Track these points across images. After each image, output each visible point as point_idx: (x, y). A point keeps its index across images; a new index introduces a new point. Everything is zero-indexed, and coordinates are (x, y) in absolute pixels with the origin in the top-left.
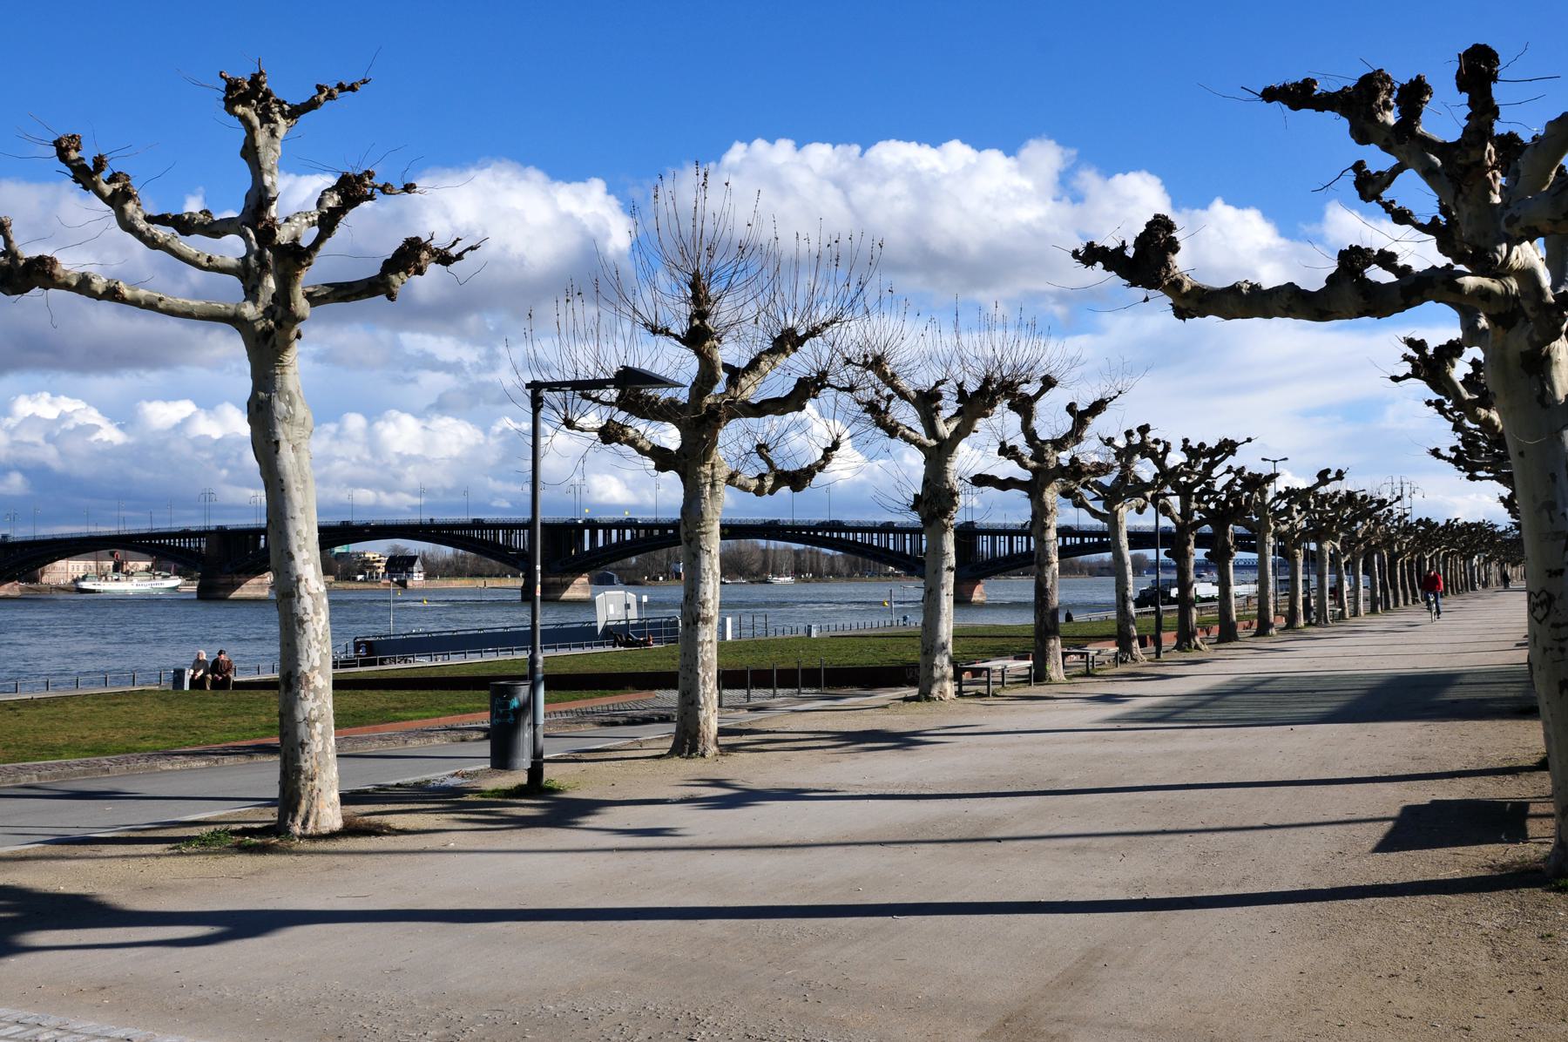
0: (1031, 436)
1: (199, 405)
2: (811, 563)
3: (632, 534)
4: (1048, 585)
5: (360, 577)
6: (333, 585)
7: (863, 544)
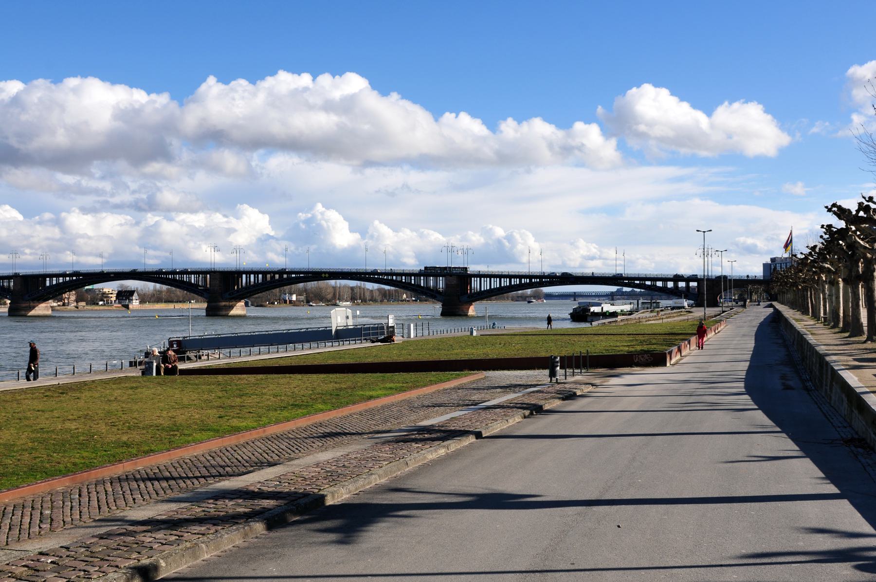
2: (360, 294)
5: (101, 303)
6: (85, 308)
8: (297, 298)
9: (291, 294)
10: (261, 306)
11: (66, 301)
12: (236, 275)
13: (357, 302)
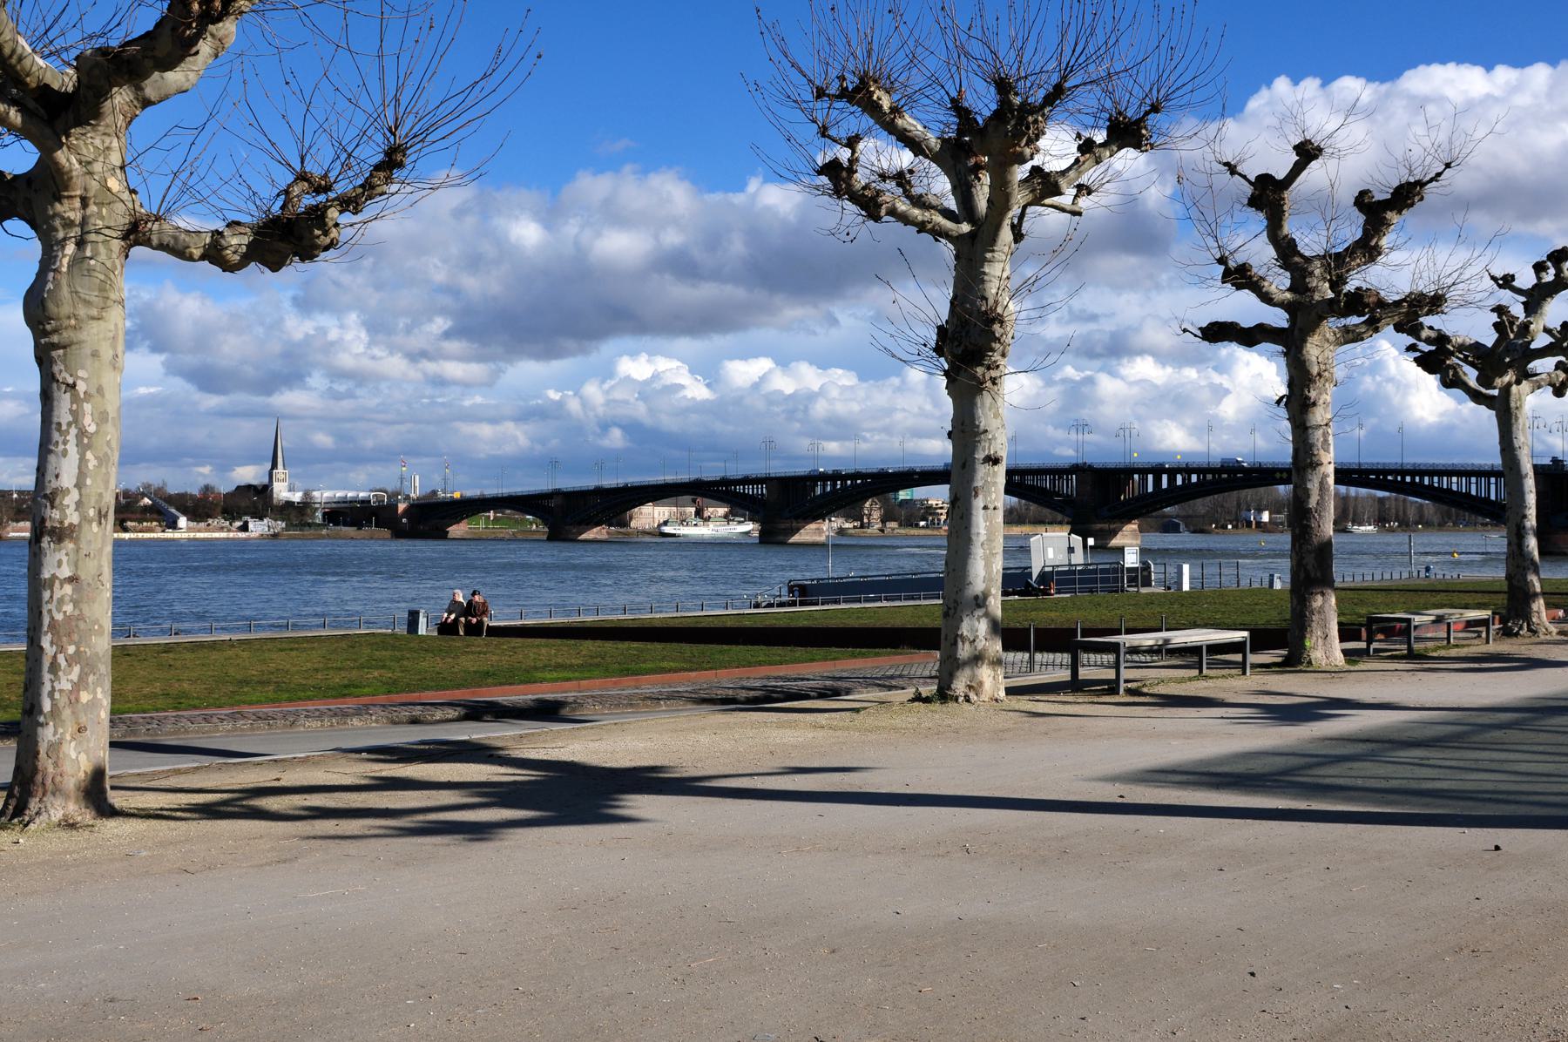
0: (1286, 251)
1: (777, 363)
2: (1397, 512)
3: (1184, 480)
4: (1313, 503)
5: (922, 523)
6: (896, 531)
7: (1440, 489)
8: (1270, 518)
9: (1260, 511)
10: (1202, 531)
11: (866, 520)
12: (1122, 476)
13: (1390, 526)
